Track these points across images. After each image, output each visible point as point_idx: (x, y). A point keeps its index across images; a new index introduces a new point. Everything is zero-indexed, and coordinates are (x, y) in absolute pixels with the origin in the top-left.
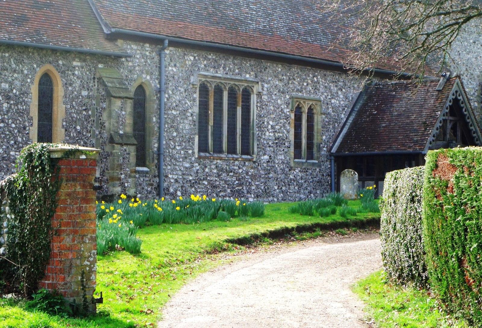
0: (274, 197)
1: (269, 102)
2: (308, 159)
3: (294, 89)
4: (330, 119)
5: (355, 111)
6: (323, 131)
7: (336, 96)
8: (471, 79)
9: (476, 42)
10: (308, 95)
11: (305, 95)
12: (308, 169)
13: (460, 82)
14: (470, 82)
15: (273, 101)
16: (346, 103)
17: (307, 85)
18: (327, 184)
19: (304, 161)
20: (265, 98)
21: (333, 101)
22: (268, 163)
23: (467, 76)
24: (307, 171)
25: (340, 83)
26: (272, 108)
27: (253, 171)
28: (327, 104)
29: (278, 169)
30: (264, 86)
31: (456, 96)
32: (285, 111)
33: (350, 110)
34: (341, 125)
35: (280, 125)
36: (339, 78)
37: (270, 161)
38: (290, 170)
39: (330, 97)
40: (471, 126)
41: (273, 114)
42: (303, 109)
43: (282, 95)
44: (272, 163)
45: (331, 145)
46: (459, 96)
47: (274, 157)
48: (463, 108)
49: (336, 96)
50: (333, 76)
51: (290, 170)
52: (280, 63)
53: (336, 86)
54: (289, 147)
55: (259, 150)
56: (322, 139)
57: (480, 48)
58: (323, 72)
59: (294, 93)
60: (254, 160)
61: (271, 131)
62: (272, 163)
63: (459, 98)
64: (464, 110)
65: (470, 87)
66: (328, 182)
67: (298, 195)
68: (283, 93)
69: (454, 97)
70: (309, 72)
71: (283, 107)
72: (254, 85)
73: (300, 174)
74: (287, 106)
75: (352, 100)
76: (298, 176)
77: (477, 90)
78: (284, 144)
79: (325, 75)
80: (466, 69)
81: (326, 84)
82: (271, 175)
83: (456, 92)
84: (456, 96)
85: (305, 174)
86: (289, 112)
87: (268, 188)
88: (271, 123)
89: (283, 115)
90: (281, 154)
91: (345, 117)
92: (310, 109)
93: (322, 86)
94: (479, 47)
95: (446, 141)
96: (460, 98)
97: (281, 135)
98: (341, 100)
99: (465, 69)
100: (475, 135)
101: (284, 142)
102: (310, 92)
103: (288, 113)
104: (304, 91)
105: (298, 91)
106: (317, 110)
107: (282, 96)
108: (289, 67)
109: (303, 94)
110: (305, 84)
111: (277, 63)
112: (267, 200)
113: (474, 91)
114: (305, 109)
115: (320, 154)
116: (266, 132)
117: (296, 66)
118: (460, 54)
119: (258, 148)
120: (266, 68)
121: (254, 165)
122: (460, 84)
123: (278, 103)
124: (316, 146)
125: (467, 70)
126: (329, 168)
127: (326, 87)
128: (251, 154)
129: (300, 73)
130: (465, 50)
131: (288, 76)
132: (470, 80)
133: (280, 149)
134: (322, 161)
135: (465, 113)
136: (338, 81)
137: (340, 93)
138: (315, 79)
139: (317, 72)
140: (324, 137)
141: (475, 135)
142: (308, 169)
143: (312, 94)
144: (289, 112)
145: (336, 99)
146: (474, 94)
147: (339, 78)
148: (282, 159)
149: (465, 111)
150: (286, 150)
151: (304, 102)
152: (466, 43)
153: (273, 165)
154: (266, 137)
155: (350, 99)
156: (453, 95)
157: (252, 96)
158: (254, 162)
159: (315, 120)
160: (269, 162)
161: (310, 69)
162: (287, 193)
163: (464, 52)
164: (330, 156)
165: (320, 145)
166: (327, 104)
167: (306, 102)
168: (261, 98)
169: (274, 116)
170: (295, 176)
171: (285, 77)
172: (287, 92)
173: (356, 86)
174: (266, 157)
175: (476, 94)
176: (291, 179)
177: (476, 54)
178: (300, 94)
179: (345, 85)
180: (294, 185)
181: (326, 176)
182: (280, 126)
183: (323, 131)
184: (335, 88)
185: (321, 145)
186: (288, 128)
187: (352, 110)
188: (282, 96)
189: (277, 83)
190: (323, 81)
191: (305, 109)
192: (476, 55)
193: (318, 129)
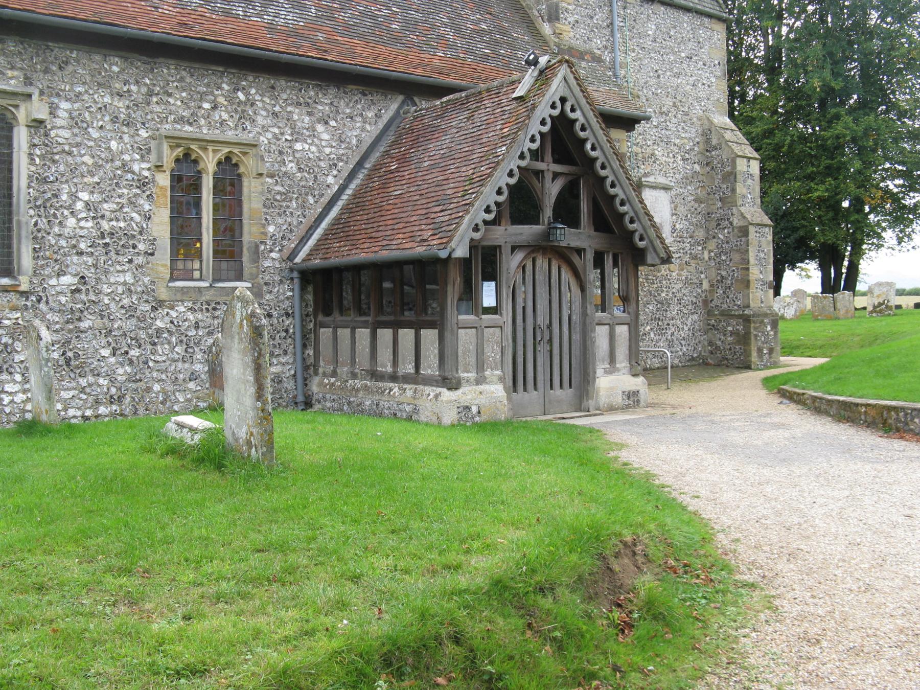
0: (98, 375)
1: (78, 145)
2: (215, 280)
3: (167, 118)
4: (290, 185)
5: (366, 169)
6: (266, 213)
7: (309, 136)
8: (684, 122)
9: (695, 58)
10: (218, 131)
11: (205, 131)
12: (218, 303)
13: (572, 76)
14: (683, 128)
15: (92, 144)
16: (341, 152)
17: (215, 108)
18: (284, 334)
19: (206, 284)
20: (62, 135)
21: (298, 146)
22: (77, 295)
23: (675, 117)
24: (215, 309)
25: (321, 108)
26: (88, 159)
27: (19, 315)
28: (281, 153)
29: (113, 306)
30: (57, 107)
31: (563, 111)
32: (136, 168)
33: (352, 166)
34: (325, 200)
35: (118, 200)
36: (317, 94)
37: (84, 289)
38: (154, 309)
39: (289, 138)
40: (613, 185)
41: (93, 176)
42: (201, 166)
43: (125, 129)
44: (91, 293)
45: (293, 246)
46: (573, 110)
47: (98, 280)
48: (585, 141)
49: (309, 136)
50: (300, 90)
51: (154, 309)
52: (113, 53)
53: (310, 114)
54: (152, 254)
55: (41, 263)
56: (265, 234)
57: (702, 69)
58: (265, 81)
59: (167, 127)
60: (24, 287)
61: (83, 215)
62: (91, 293)
63: (572, 116)
64: (588, 146)
65: (683, 135)
66: (287, 331)
67: (187, 365)
68: (128, 125)
69: (556, 112)
70: (221, 77)
71: (127, 157)
72: (17, 102)
73: (191, 317)
74: (142, 157)
75: (357, 147)
76: (185, 320)
77: (698, 143)
78: (134, 247)
79: (273, 88)
80: (674, 103)
81: (277, 109)
82: (85, 324)
83: (563, 100)
84: (563, 111)
85: (209, 315)
86: (149, 169)
87: (77, 356)
88: (85, 196)
89: (129, 176)
90: (123, 271)
91: (336, 183)
92: (228, 167)
93: (264, 113)
94: (699, 66)
95: (543, 224)
96: (577, 115)
97: (122, 224)
98: (324, 143)
99: (671, 104)
100: (625, 208)
101: (131, 242)
102: (221, 124)
103: (146, 173)
104: (202, 122)
105: (181, 120)
106: (249, 165)
107: (124, 133)
108: (149, 63)
109: (200, 127)
110: (206, 106)
111: (104, 51)
112: (74, 384)
113: (691, 144)
114: (210, 163)
115: (257, 267)
116: (66, 218)
117: (173, 62)
118: (659, 76)
119: (36, 258)
120: (67, 63)
121: (23, 302)
122: (573, 82)
123: (109, 149)
124: (248, 249)
125: (675, 105)
126: (288, 298)
127: (275, 115)
128: (16, 274)
129: (188, 80)
130: (671, 70)
131: (146, 84)
132: (683, 124)
133: (120, 258)
134: (266, 284)
135: (593, 154)
136: (315, 102)
137: (320, 128)
138: (241, 95)
139: (245, 80)
140: (271, 229)
141: (625, 208)
142: (218, 303)
143: (231, 129)
144: (149, 169)
145: (309, 141)
146: (692, 149)
147: (317, 94)
148: (125, 283)
149: (593, 148)
150: (140, 260)
151: (201, 148)
152: (672, 58)
153: (93, 298)
154: (67, 231)
155: (354, 142)
156: (553, 106)
157: (15, 130)
158: (25, 294)
159: (245, 190)
160: (78, 291)
161: (223, 73)
162: (146, 363)
163: (668, 74)
164: (291, 270)
165: (257, 247)
166: (281, 153)
167: (210, 148)
168: (46, 135)
169: (96, 179)
170: (172, 322)
171: (134, 88)
172: (143, 124)
173: (370, 114)
174: (68, 280)
175: (696, 149)
176: (159, 331)
177: (694, 78)
178: (187, 128)
179: (337, 112)
180: (169, 343)
181: (280, 316)
182: (118, 203)
183: (266, 213)
184: (307, 119)
185: (262, 247)
186: (147, 207)
187: (360, 164)
188: (124, 133)
189: (107, 99)
190: (267, 100)
191: (210, 163)
192: (694, 81)
193: (250, 209)
